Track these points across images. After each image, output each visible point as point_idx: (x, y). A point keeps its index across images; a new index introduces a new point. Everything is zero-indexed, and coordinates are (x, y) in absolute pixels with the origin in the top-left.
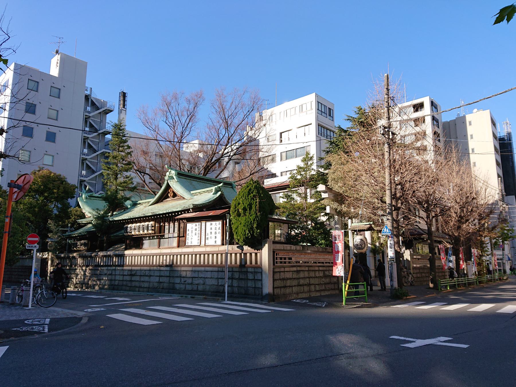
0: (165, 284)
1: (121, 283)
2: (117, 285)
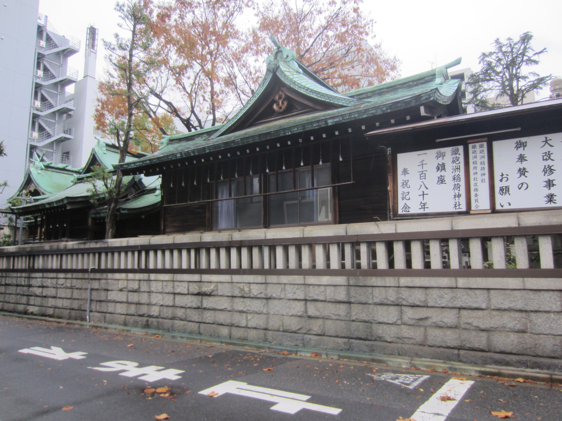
0: (329, 323)
1: (168, 312)
2: (157, 317)
